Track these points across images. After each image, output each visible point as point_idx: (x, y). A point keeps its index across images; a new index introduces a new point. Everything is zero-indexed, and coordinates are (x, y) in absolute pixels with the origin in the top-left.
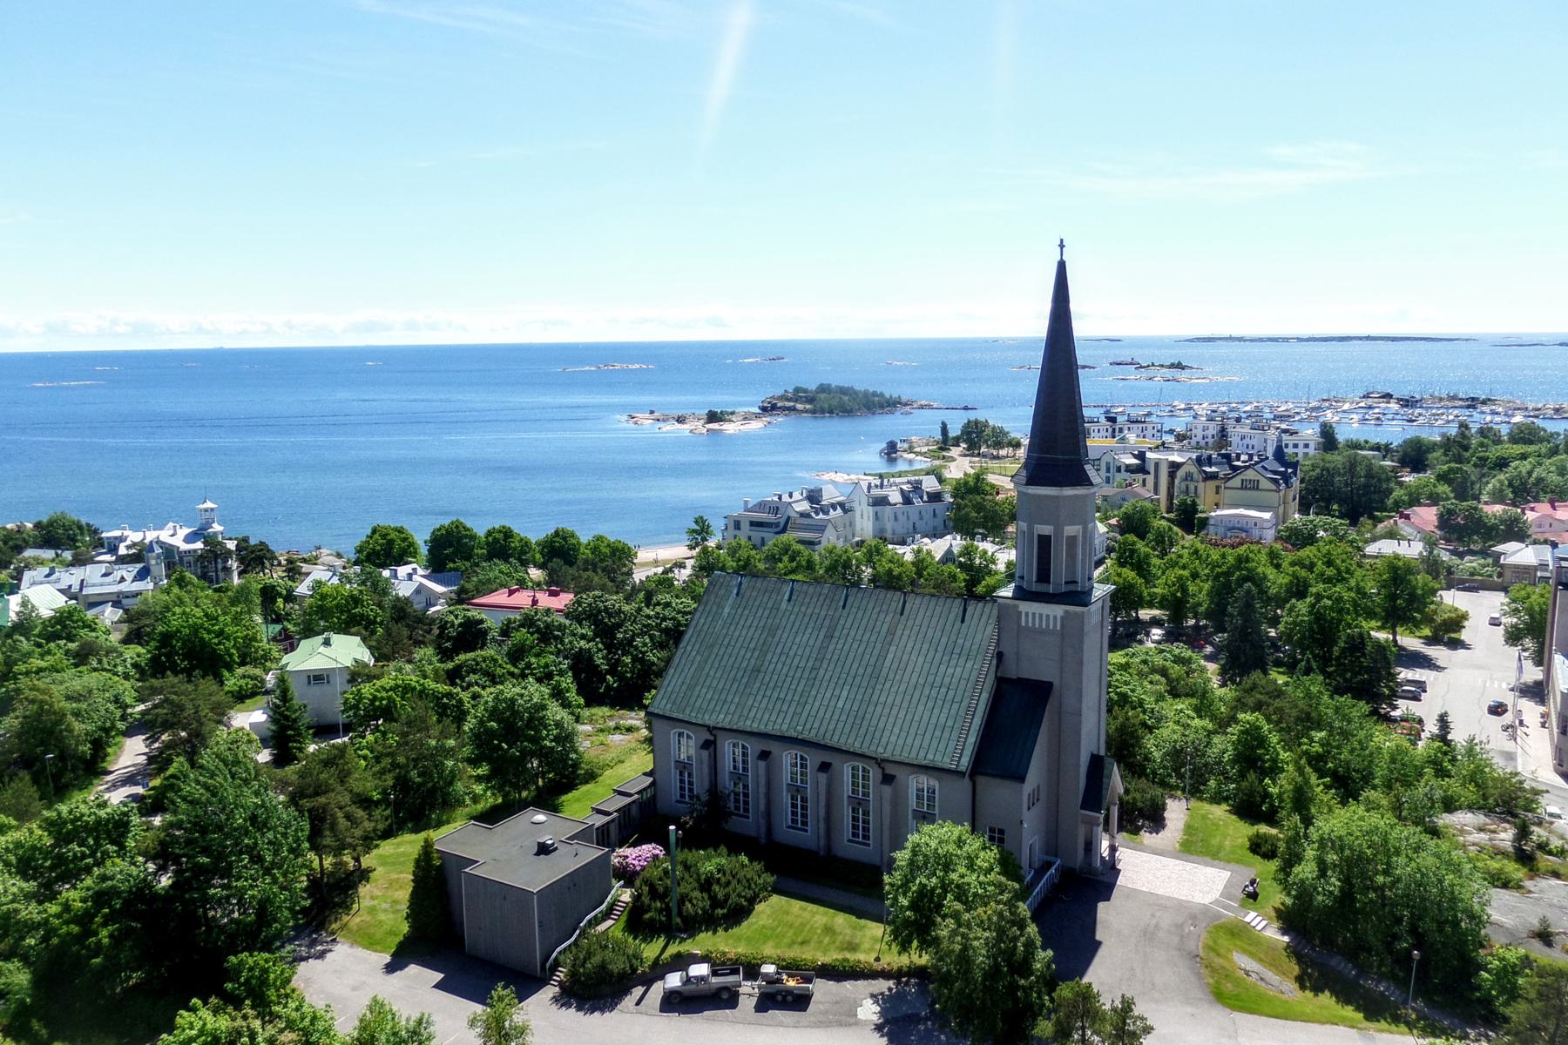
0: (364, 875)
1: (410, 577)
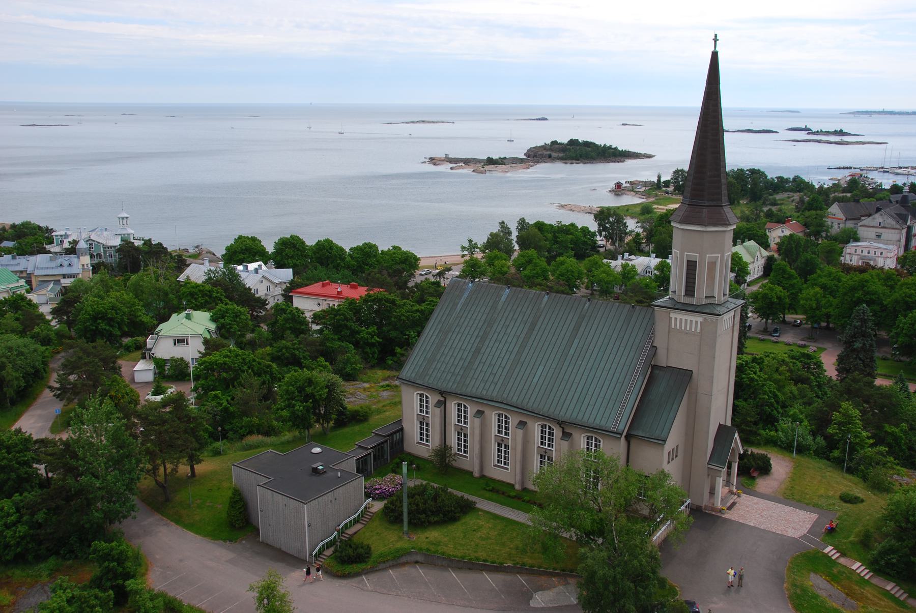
1: (256, 271)
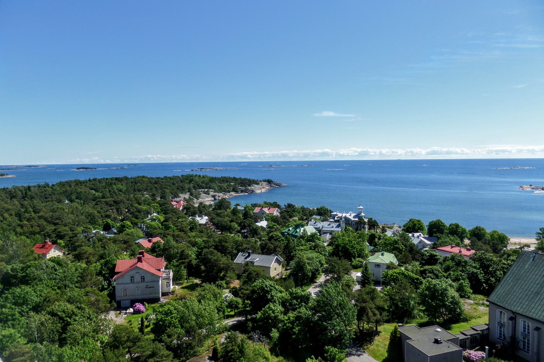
0: (377, 333)
1: (418, 237)
